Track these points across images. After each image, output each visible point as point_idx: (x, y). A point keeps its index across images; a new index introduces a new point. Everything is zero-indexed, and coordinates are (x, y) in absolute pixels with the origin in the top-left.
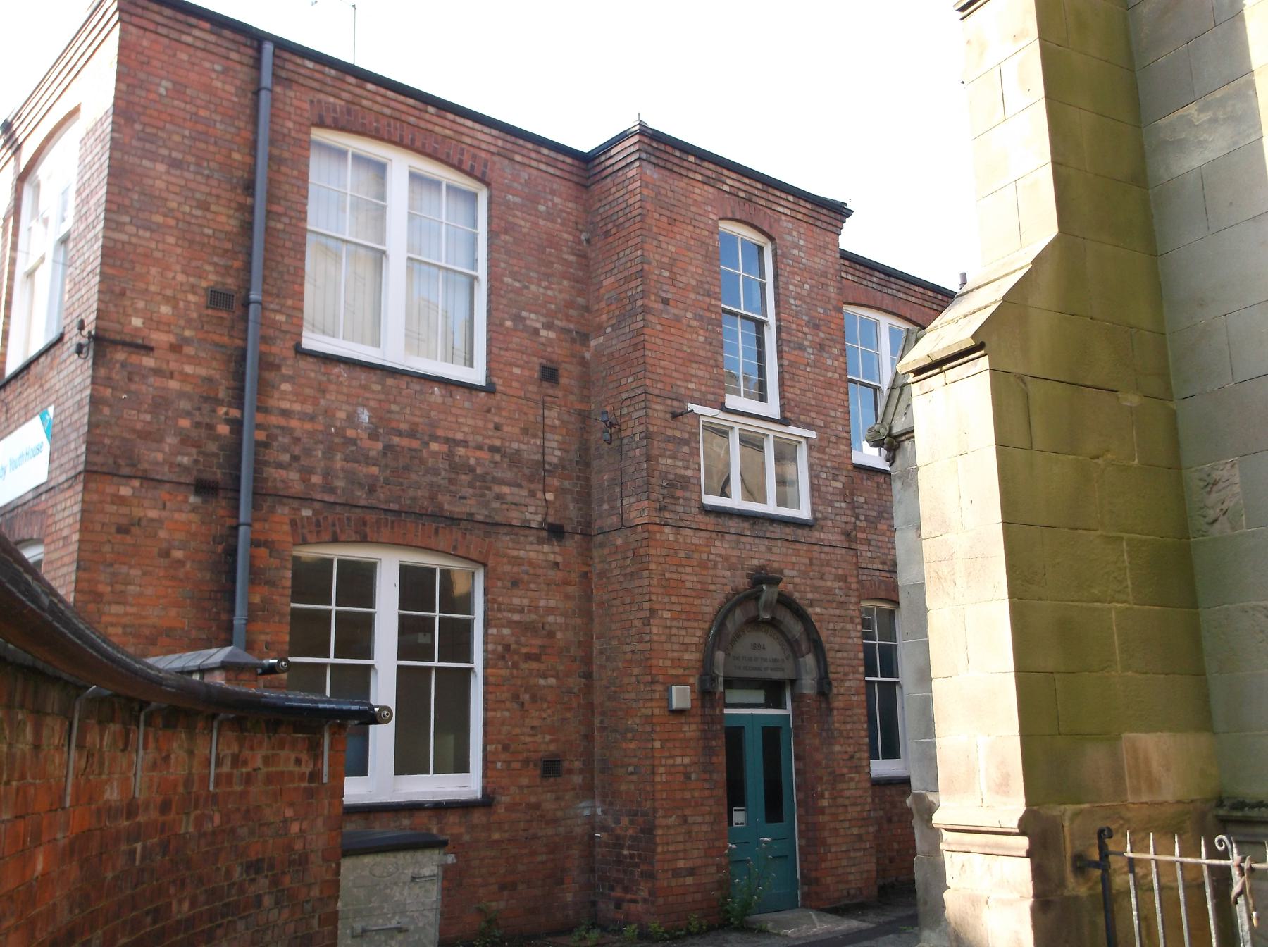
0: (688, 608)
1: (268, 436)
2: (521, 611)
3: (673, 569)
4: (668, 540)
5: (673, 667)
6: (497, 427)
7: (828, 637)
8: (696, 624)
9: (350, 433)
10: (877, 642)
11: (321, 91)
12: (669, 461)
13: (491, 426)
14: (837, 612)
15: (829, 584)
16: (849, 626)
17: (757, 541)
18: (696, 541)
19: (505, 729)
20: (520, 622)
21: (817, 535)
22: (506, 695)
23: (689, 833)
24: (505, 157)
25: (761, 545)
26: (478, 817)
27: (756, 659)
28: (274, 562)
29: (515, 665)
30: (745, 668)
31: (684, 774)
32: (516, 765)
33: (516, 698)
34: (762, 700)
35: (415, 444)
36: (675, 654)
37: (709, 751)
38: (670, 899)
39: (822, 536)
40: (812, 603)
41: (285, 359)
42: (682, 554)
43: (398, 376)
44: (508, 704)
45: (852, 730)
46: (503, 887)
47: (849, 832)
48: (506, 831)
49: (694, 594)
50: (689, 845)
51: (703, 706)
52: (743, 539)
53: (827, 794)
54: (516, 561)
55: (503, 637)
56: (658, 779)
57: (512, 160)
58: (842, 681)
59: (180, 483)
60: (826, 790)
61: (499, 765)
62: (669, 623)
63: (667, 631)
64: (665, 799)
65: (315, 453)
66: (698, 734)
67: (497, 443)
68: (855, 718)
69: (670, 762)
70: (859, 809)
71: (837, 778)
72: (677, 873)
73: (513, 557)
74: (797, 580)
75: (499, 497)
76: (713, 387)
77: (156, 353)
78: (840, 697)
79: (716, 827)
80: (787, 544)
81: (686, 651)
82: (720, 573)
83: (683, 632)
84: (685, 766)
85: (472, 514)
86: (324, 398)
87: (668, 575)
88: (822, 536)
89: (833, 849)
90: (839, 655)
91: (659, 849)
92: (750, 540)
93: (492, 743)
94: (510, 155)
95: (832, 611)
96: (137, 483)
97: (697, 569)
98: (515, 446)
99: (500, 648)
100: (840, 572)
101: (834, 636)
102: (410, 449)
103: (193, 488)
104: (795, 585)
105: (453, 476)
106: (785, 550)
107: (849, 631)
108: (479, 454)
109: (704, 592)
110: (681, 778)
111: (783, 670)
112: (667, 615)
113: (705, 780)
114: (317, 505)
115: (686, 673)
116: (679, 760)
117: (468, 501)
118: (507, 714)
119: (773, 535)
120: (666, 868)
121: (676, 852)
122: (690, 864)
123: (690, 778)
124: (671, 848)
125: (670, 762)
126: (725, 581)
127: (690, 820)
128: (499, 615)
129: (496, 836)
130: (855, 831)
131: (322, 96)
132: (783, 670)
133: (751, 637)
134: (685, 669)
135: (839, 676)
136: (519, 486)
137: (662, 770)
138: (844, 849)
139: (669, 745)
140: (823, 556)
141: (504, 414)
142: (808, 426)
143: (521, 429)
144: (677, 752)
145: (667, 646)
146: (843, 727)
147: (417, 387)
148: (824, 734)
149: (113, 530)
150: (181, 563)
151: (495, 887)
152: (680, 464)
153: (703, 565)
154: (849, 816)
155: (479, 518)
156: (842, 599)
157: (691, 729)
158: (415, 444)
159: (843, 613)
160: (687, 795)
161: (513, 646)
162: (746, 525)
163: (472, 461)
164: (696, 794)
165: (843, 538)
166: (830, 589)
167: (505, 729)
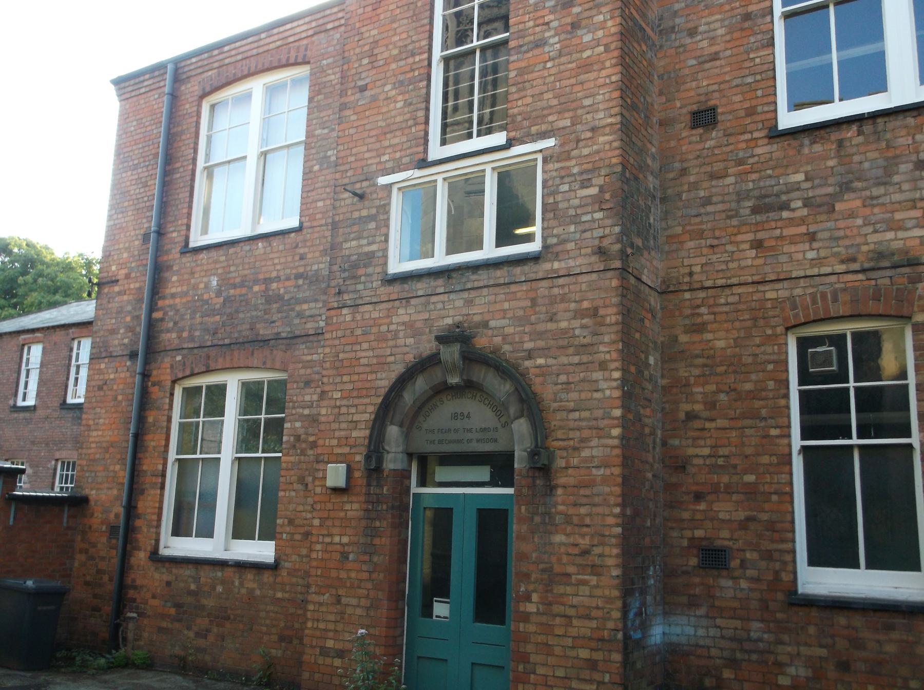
0: (360, 385)
1: (164, 314)
2: (311, 407)
3: (348, 348)
4: (345, 322)
5: (339, 446)
6: (302, 258)
7: (555, 394)
8: (367, 401)
9: (206, 297)
10: (852, 384)
11: (203, 72)
12: (354, 243)
13: (297, 258)
14: (576, 359)
15: (564, 325)
16: (597, 375)
17: (452, 296)
18: (375, 315)
19: (292, 507)
20: (309, 415)
21: (546, 266)
22: (294, 478)
23: (342, 613)
24: (321, 32)
25: (458, 301)
26: (267, 577)
27: (456, 431)
28: (161, 394)
29: (303, 453)
30: (441, 442)
31: (341, 553)
32: (298, 537)
33: (301, 480)
34: (487, 478)
35: (244, 291)
36: (343, 433)
37: (372, 532)
38: (317, 676)
39: (556, 265)
40: (530, 355)
41: (175, 260)
42: (359, 332)
43: (236, 244)
44: (296, 486)
45: (589, 515)
46: (282, 638)
47: (573, 653)
48: (287, 592)
49: (368, 369)
50: (340, 627)
51: (369, 485)
52: (434, 299)
53: (535, 597)
54: (309, 364)
55: (295, 429)
56: (314, 555)
57: (326, 31)
58: (576, 449)
59: (123, 355)
60: (535, 591)
61: (284, 536)
62: (338, 403)
63: (336, 410)
64: (321, 576)
65: (186, 317)
66: (361, 513)
67: (301, 270)
68: (597, 500)
69: (328, 540)
70: (594, 624)
71: (552, 578)
72: (325, 652)
73: (308, 361)
74: (510, 330)
75: (300, 315)
76: (410, 148)
77: (120, 283)
78: (570, 471)
79: (372, 613)
80: (497, 290)
81: (355, 429)
82: (401, 342)
83: (353, 410)
84: (343, 545)
85: (279, 333)
86: (194, 278)
87: (341, 356)
88: (556, 265)
89: (541, 670)
90: (576, 415)
91: (309, 624)
92: (444, 298)
93: (281, 518)
94: (323, 28)
95: (564, 360)
96: (106, 360)
97: (374, 344)
98: (315, 267)
99: (292, 439)
100: (586, 304)
101: (568, 391)
102: (240, 296)
103: (128, 357)
104: (505, 337)
105: (267, 307)
106: (492, 298)
107: (596, 381)
108: (288, 283)
109: (383, 364)
110: (337, 556)
111: (496, 441)
112: (337, 395)
113: (365, 562)
114: (185, 352)
115: (352, 451)
116: (337, 539)
117: (277, 324)
118: (293, 494)
119: (476, 284)
120: (314, 643)
121: (326, 630)
122: (340, 646)
123: (348, 558)
124: (322, 626)
125: (328, 540)
126: (407, 349)
127: (344, 600)
128: (294, 412)
129: (279, 595)
130: (584, 654)
131: (206, 75)
132: (496, 441)
133: (449, 407)
134: (351, 447)
135: (571, 443)
136: (316, 301)
137: (319, 547)
138: (560, 673)
139: (329, 523)
140: (556, 291)
141: (308, 244)
142: (543, 136)
143: (321, 251)
144: (335, 531)
145: (335, 426)
146: (571, 511)
147: (248, 248)
148: (537, 519)
149: (96, 389)
150: (121, 402)
151: (275, 638)
152: (365, 242)
153: (381, 338)
154: (573, 632)
155: (284, 335)
156: (587, 340)
157: (353, 508)
158: (244, 291)
159: (585, 359)
160: (343, 575)
161: (303, 437)
162: (440, 282)
163: (282, 291)
164: (353, 575)
165: (594, 259)
166: (564, 331)
167: (292, 507)
